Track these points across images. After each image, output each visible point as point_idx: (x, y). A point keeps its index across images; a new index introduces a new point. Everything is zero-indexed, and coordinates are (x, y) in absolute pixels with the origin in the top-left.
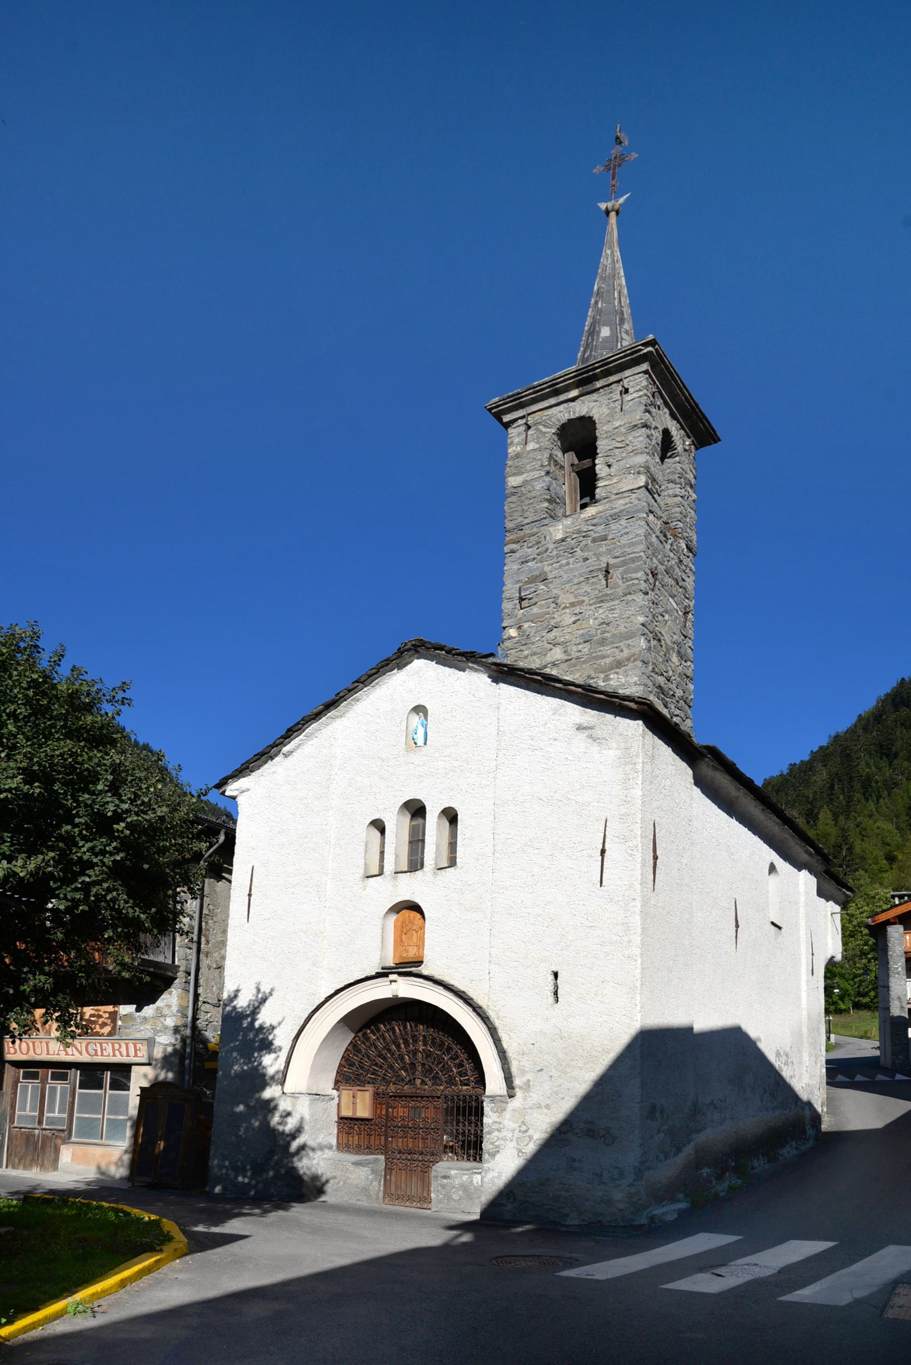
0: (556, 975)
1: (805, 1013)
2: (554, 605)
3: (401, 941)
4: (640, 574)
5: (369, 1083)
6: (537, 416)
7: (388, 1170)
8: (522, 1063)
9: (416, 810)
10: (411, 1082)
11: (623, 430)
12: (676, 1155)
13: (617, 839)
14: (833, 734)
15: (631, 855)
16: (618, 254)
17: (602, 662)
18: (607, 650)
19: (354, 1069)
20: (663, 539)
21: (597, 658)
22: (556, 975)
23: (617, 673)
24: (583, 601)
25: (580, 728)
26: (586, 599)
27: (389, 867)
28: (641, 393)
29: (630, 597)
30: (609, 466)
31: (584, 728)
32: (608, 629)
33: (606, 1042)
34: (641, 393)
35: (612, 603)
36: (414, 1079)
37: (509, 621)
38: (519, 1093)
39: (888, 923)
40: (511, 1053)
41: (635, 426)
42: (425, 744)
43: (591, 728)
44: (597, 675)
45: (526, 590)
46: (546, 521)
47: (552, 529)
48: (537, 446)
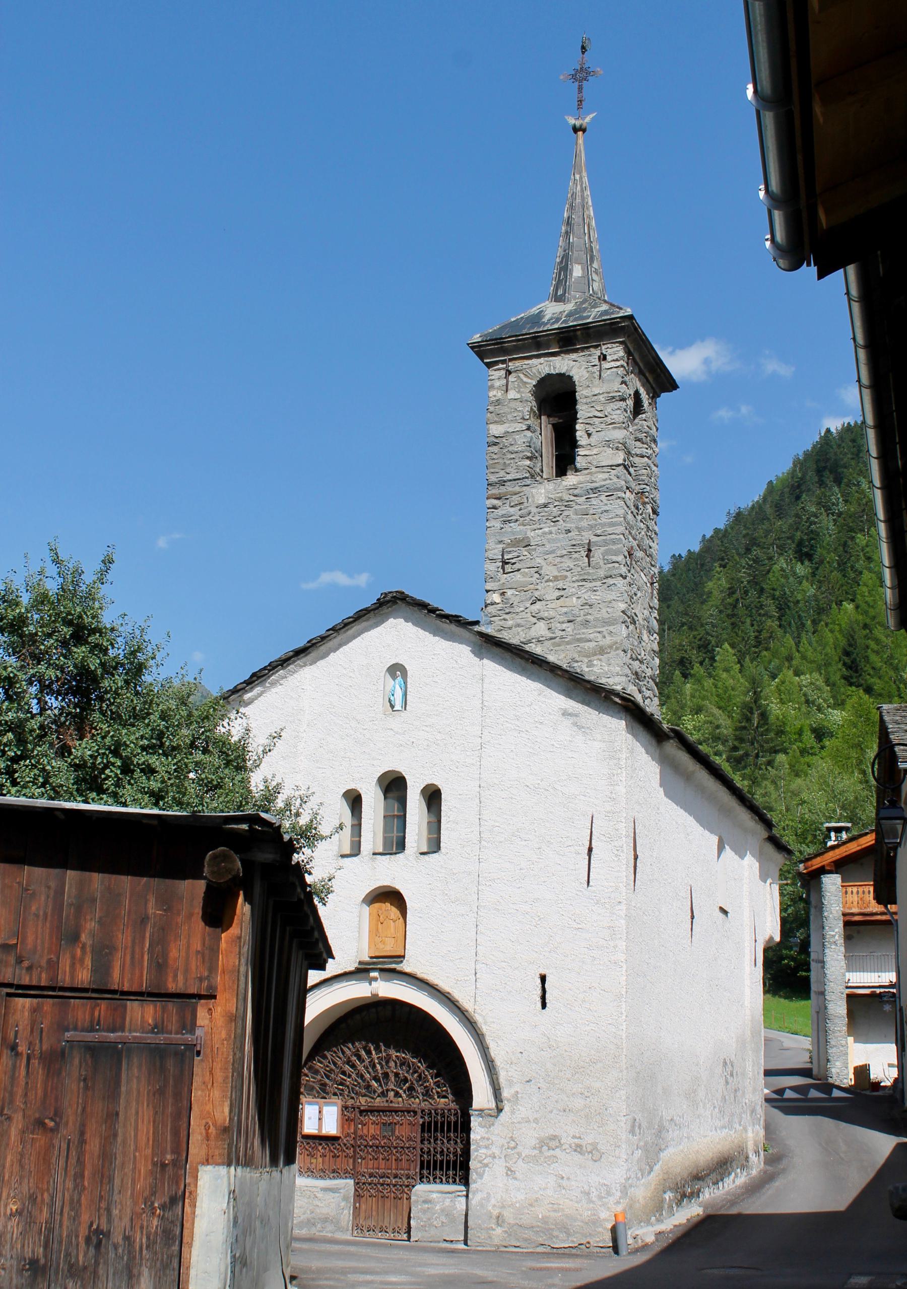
0: (543, 979)
1: (748, 1012)
2: (538, 576)
3: (377, 930)
4: (620, 558)
5: (335, 1094)
6: (518, 363)
7: (358, 1196)
9: (393, 785)
10: (384, 1094)
11: (602, 398)
12: (649, 1173)
13: (603, 838)
14: (733, 511)
15: (617, 856)
16: (585, 179)
17: (587, 645)
18: (589, 633)
19: (319, 1077)
20: (635, 511)
21: (579, 640)
22: (543, 979)
23: (600, 660)
24: (566, 577)
25: (565, 714)
26: (568, 574)
27: (367, 845)
28: (618, 364)
29: (610, 581)
30: (589, 435)
31: (569, 714)
33: (593, 1052)
34: (618, 364)
35: (594, 584)
36: (387, 1090)
37: (492, 584)
38: (507, 1108)
39: (822, 871)
40: (499, 1062)
41: (613, 397)
43: (576, 715)
44: (581, 659)
45: (510, 552)
46: (528, 482)
47: (534, 491)
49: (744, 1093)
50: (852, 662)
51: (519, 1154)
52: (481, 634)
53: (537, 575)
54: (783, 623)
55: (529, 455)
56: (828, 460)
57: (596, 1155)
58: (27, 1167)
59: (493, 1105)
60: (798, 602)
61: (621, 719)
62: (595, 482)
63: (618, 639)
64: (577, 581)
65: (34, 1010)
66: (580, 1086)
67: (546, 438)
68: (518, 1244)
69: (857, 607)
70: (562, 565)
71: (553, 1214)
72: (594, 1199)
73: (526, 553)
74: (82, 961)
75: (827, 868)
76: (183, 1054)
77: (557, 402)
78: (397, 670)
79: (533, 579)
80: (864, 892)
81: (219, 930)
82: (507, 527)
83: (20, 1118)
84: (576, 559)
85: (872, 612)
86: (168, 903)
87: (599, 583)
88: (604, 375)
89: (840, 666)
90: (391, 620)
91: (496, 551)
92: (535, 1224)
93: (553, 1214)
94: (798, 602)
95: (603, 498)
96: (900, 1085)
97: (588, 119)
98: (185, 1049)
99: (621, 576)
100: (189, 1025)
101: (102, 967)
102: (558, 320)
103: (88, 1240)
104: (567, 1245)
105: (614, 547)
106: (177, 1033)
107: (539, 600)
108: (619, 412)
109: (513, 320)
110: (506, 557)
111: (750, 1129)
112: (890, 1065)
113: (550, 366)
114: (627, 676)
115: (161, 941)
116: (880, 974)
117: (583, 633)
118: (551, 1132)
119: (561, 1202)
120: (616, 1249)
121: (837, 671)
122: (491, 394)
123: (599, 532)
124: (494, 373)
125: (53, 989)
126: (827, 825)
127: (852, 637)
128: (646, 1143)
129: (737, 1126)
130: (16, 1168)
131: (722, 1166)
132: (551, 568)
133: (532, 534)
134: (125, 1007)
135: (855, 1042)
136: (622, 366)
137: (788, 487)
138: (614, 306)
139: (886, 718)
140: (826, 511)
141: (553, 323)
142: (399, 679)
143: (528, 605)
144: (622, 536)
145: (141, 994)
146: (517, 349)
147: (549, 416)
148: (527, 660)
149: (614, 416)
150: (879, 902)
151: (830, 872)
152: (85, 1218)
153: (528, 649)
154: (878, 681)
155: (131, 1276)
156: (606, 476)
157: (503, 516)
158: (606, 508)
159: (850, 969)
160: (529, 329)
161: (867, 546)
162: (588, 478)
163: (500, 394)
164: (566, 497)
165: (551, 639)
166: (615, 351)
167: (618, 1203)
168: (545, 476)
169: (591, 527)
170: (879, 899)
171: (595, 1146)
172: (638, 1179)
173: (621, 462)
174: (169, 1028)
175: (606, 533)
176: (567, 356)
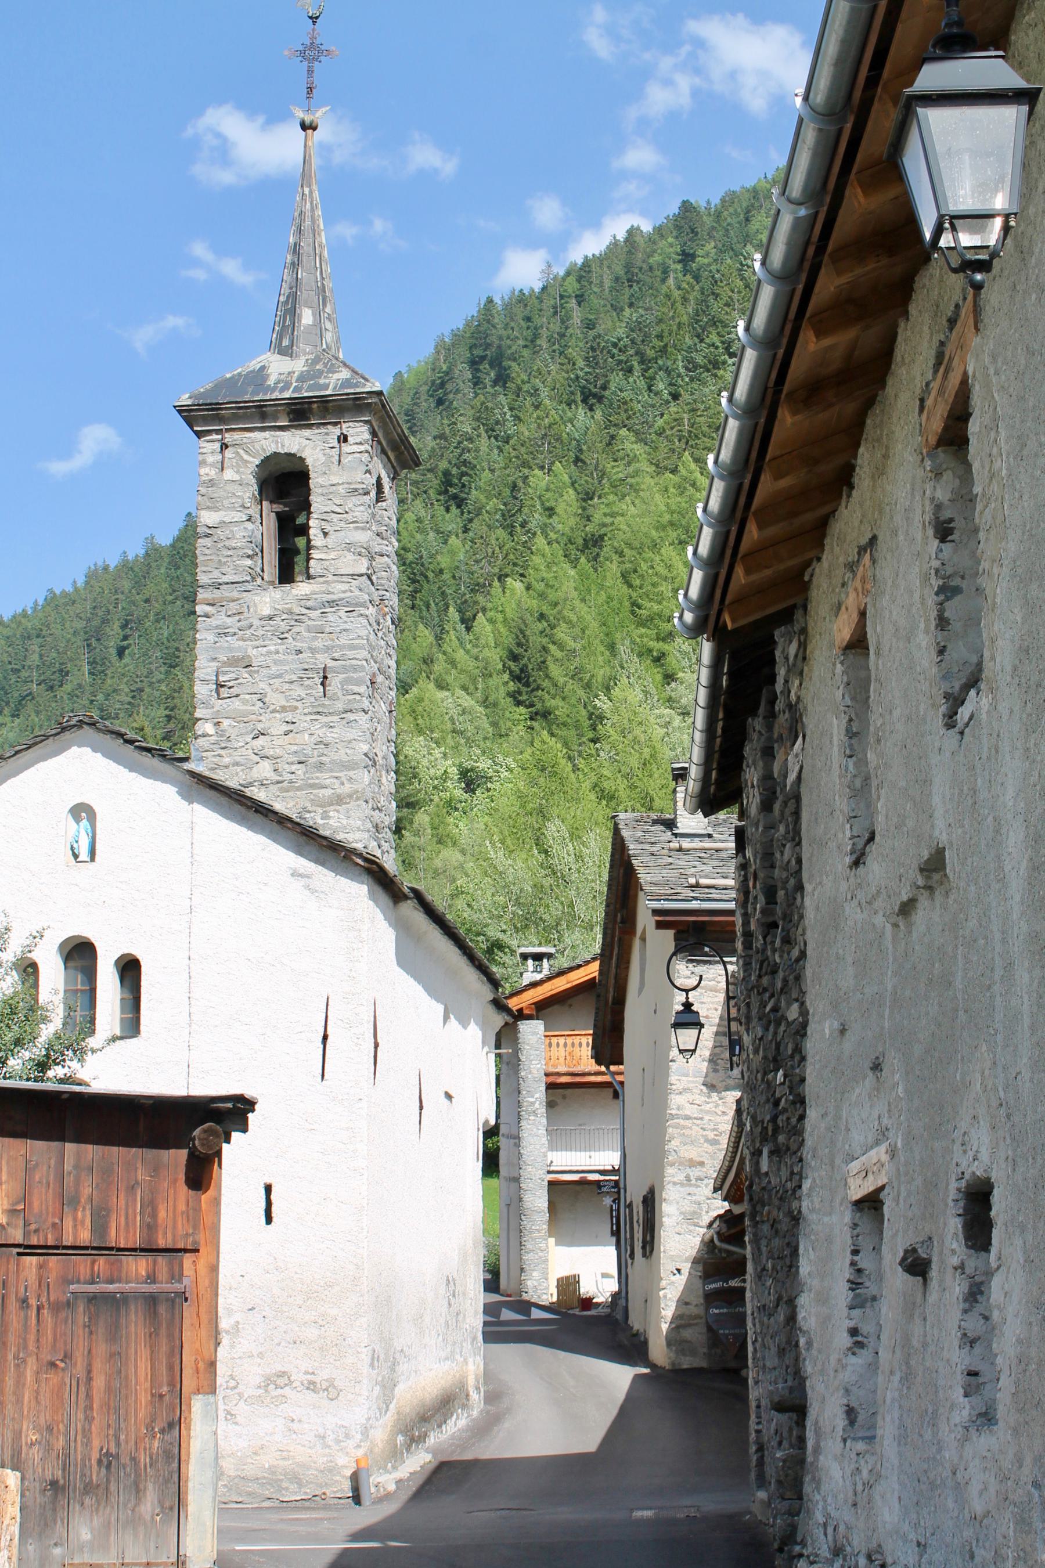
0: (268, 1189)
6: (237, 436)
9: (80, 953)
11: (341, 489)
17: (322, 792)
18: (324, 778)
20: (376, 627)
21: (313, 786)
22: (268, 1189)
23: (338, 811)
24: (296, 708)
25: (295, 874)
28: (362, 448)
29: (351, 716)
30: (325, 534)
31: (300, 875)
34: (362, 448)
35: (330, 718)
37: (204, 711)
41: (356, 490)
46: (249, 587)
47: (257, 599)
49: (465, 1315)
50: (522, 670)
51: (240, 1395)
52: (192, 774)
53: (260, 704)
54: (418, 602)
55: (250, 552)
56: (488, 346)
57: (333, 1393)
58: (43, 1402)
60: (441, 571)
61: (363, 883)
62: (333, 593)
63: (359, 787)
64: (310, 713)
65: (41, 1267)
66: (314, 1313)
67: (268, 530)
68: (240, 1500)
69: (528, 588)
70: (291, 693)
71: (282, 1463)
72: (330, 1443)
73: (247, 675)
74: (83, 1223)
75: (526, 1012)
76: (173, 1301)
77: (285, 486)
78: (82, 812)
79: (256, 708)
80: (573, 1045)
81: (200, 1193)
82: (223, 642)
83: (34, 1360)
84: (309, 687)
85: (552, 596)
86: (156, 1169)
87: (336, 718)
88: (344, 461)
89: (506, 677)
90: (75, 749)
91: (209, 670)
92: (260, 1475)
93: (282, 1463)
94: (441, 571)
95: (342, 613)
96: (623, 1302)
97: (319, 114)
98: (175, 1297)
99: (364, 711)
100: (177, 1275)
101: (100, 1226)
102: (286, 388)
103: (100, 1462)
104: (298, 1498)
105: (355, 676)
106: (167, 1283)
107: (263, 734)
108: (362, 508)
109: (228, 376)
110: (221, 679)
111: (471, 1360)
112: (605, 1275)
113: (277, 442)
114: (369, 831)
115: (151, 1206)
116: (592, 1153)
117: (317, 778)
118: (280, 1368)
119: (292, 1449)
120: (357, 1499)
121: (501, 685)
122: (203, 471)
123: (336, 655)
124: (205, 444)
125: (57, 1247)
126: (523, 950)
127: (522, 632)
128: (384, 1377)
129: (458, 1357)
130: (33, 1404)
131: (446, 1404)
132: (277, 695)
133: (255, 652)
134: (121, 1261)
135: (556, 1245)
136: (367, 452)
137: (425, 383)
138: (356, 373)
139: (625, 833)
140: (487, 432)
141: (282, 390)
142: (85, 823)
143: (249, 740)
144: (364, 662)
145: (134, 1250)
146: (236, 418)
147: (271, 502)
148: (249, 808)
149: (357, 514)
150: (599, 1062)
151: (530, 1017)
152: (96, 1443)
153: (248, 794)
154: (561, 703)
155: (138, 1491)
156: (345, 587)
157: (217, 627)
158: (345, 626)
159: (552, 1147)
160: (253, 393)
161: (547, 490)
162: (324, 588)
163: (213, 473)
164: (297, 610)
165: (278, 782)
166: (358, 432)
167: (359, 1446)
168: (266, 578)
169: (327, 649)
170: (599, 1056)
171: (331, 1383)
172: (377, 1420)
173: (364, 571)
174: (160, 1278)
175: (346, 657)
176: (298, 432)
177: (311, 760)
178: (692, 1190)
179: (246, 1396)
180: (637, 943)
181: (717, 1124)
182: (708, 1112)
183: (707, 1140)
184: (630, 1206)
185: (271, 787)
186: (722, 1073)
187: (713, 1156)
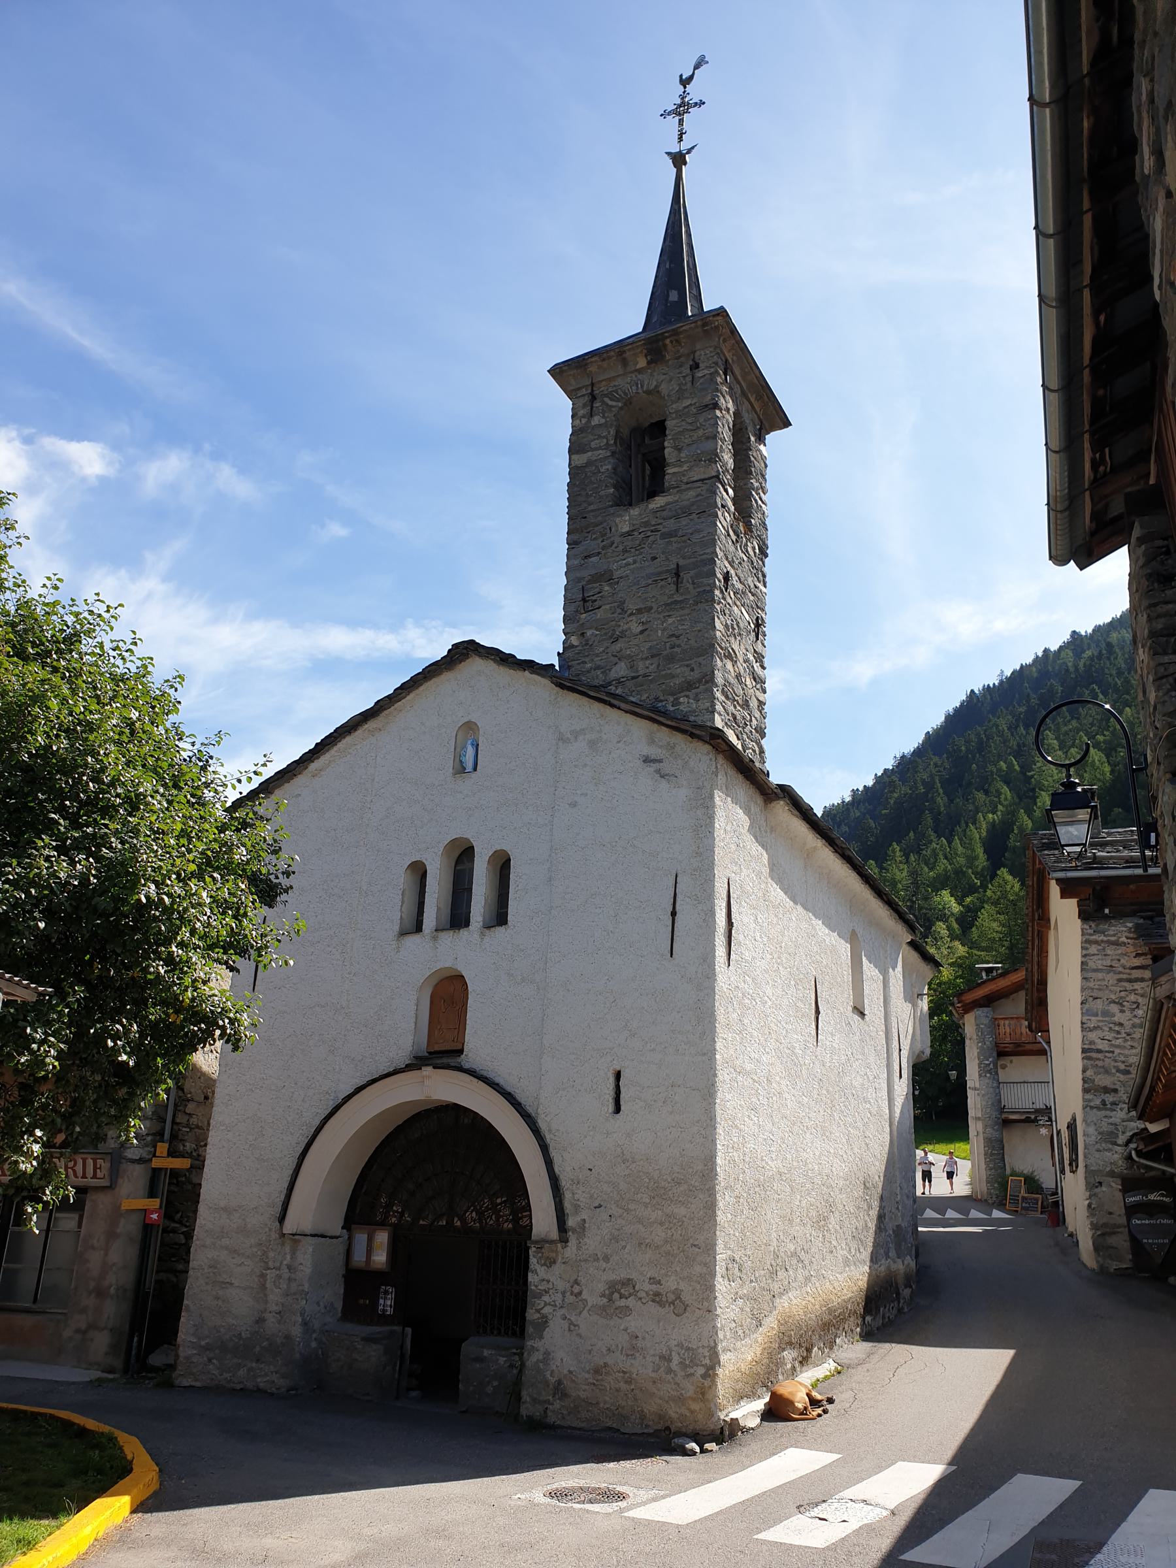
0: (618, 1075)
8: (576, 1197)
13: (688, 900)
22: (618, 1075)
23: (687, 696)
25: (647, 760)
27: (429, 921)
32: (677, 642)
35: (682, 612)
40: (564, 1182)
42: (475, 769)
43: (660, 761)
47: (618, 520)
48: (603, 421)
59: (554, 1234)
177: (665, 653)
178: (1108, 1113)
179: (590, 1304)
180: (1052, 933)
181: (1126, 1056)
182: (1118, 1047)
183: (1118, 1071)
184: (1059, 1132)
185: (628, 683)
186: (1128, 1013)
187: (1123, 1084)
